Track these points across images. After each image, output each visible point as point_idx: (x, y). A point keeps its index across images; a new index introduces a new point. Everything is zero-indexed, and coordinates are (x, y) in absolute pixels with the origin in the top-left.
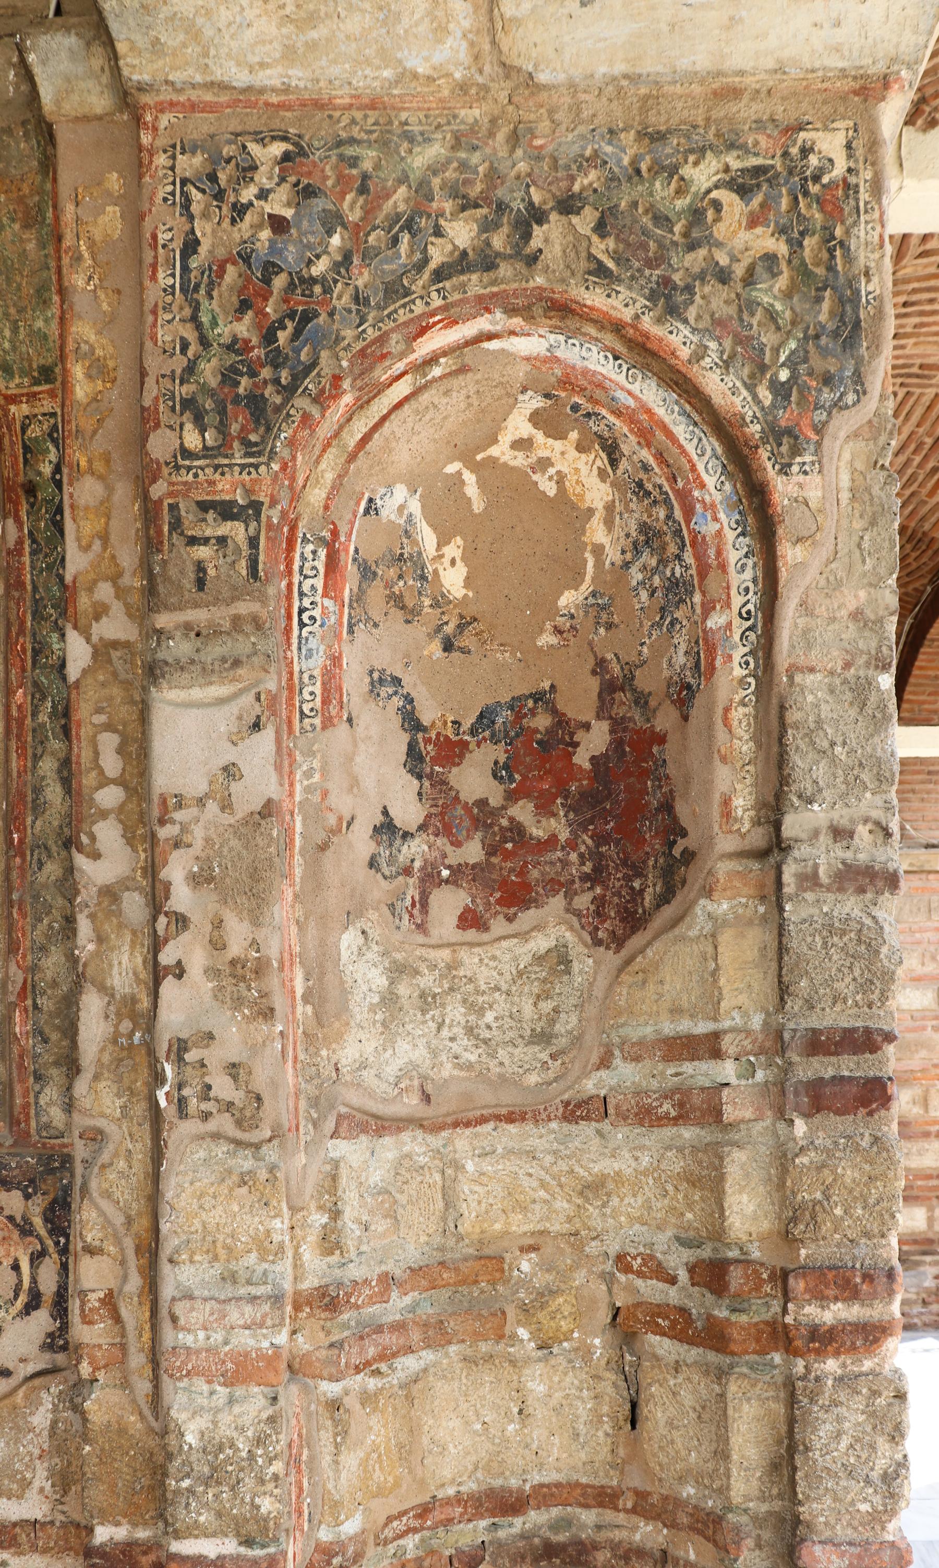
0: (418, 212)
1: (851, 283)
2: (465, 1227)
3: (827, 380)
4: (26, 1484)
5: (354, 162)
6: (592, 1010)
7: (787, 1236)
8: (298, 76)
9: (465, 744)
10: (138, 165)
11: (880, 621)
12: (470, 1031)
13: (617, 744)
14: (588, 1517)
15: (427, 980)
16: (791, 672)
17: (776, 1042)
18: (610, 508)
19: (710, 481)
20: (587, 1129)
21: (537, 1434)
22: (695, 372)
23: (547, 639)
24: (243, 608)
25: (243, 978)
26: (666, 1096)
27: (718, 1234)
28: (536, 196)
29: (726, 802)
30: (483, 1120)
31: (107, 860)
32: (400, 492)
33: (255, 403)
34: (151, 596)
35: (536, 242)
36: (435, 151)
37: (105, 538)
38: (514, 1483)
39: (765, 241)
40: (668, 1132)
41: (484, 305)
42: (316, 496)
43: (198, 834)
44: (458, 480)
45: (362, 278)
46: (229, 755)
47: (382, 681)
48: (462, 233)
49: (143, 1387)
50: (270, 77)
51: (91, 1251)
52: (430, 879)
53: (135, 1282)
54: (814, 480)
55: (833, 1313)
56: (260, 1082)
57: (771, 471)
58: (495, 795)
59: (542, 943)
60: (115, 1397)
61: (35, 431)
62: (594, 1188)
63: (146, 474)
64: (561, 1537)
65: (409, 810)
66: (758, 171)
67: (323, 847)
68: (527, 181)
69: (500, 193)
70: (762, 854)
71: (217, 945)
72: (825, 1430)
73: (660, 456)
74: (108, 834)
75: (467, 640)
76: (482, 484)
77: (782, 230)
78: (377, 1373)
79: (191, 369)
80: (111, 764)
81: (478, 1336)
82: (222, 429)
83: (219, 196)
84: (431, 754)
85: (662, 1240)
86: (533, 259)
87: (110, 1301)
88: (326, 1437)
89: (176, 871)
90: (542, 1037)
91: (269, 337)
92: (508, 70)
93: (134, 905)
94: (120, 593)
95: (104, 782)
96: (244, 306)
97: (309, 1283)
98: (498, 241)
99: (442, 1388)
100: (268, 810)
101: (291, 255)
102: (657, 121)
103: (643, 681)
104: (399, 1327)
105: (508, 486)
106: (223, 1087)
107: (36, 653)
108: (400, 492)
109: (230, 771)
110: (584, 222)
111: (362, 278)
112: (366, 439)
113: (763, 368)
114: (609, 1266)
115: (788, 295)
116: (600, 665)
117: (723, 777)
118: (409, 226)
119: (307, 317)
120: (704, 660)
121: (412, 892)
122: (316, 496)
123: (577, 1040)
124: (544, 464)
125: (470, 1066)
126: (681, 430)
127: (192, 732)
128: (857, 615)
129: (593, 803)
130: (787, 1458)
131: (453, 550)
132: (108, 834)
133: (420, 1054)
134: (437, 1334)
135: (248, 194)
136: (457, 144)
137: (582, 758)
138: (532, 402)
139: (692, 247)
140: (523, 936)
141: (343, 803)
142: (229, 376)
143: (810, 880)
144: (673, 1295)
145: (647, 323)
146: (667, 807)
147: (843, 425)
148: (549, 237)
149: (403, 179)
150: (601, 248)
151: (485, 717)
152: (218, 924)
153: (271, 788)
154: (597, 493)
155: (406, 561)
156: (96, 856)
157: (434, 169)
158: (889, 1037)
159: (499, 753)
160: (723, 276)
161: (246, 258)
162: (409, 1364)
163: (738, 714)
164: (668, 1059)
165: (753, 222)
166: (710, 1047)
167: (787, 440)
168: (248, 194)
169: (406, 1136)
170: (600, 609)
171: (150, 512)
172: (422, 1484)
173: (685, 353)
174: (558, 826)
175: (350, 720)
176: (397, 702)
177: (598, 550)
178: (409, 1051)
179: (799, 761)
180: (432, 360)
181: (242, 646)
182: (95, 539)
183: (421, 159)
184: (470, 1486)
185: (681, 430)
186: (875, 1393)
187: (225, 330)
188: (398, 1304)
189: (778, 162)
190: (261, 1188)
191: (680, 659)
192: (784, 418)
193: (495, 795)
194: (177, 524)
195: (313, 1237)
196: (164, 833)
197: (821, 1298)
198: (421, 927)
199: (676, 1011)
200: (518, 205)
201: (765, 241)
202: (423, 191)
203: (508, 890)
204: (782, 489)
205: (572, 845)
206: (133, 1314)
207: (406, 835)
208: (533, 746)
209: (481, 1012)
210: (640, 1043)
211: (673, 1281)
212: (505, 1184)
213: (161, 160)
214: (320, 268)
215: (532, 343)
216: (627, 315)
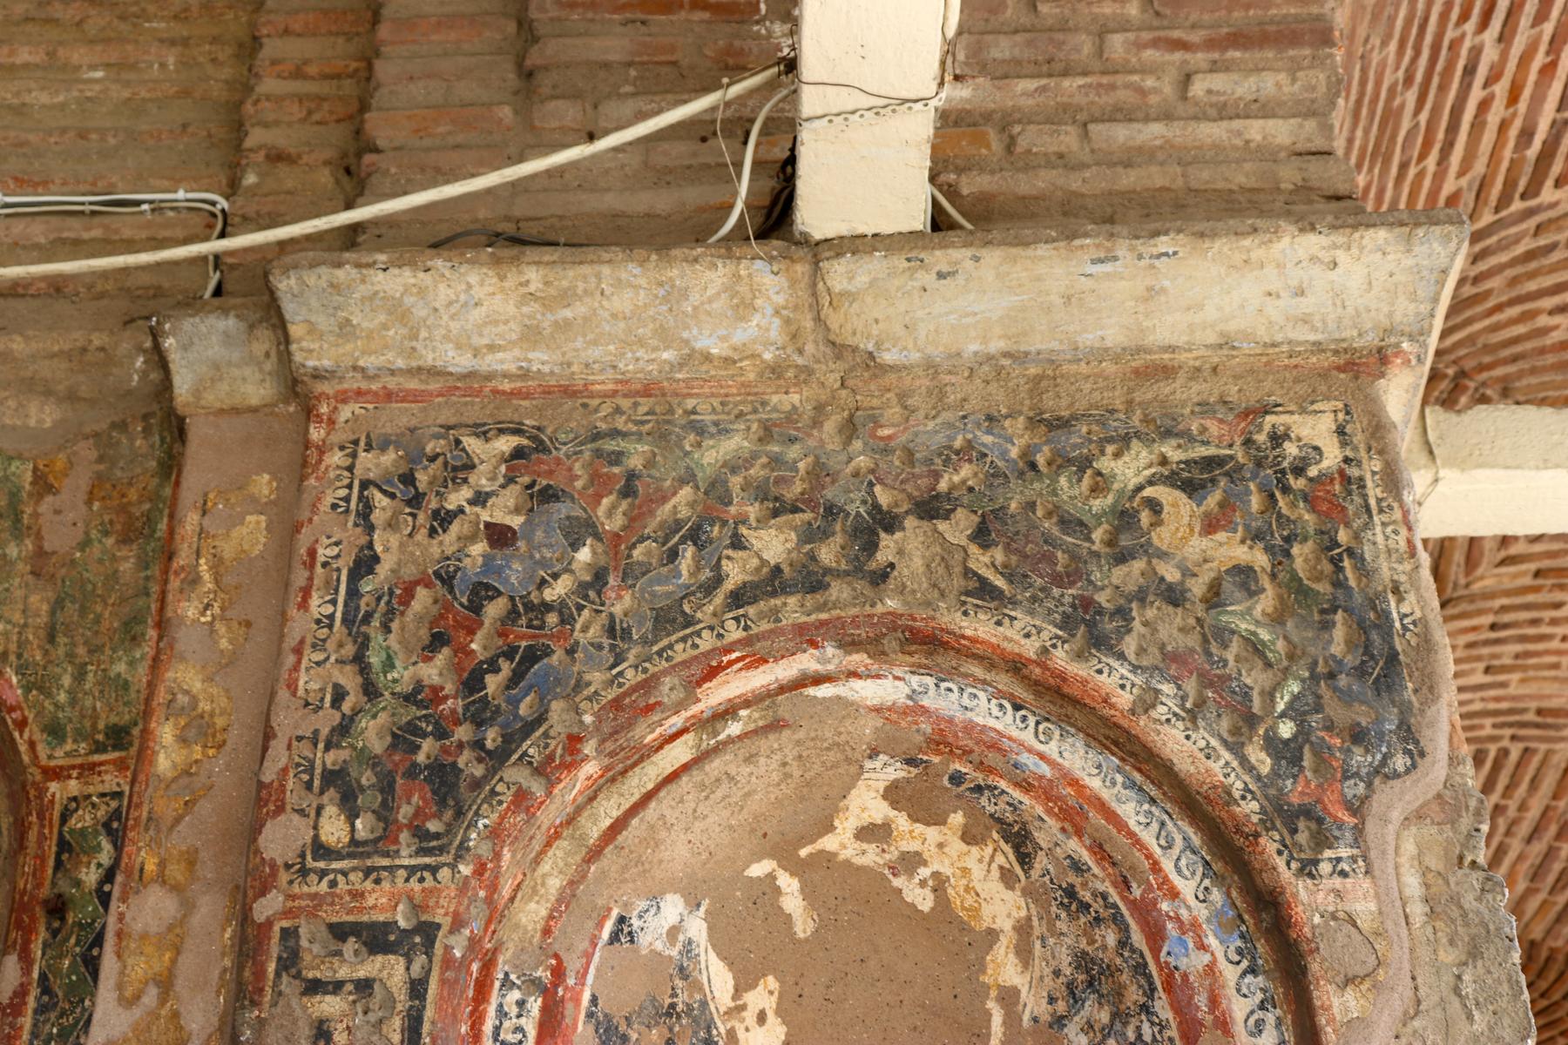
3: (1358, 736)
5: (616, 458)
8: (541, 360)
10: (304, 461)
18: (1023, 928)
19: (1187, 888)
28: (884, 497)
32: (673, 908)
33: (443, 779)
35: (884, 555)
36: (736, 443)
37: (166, 984)
41: (807, 637)
42: (531, 914)
45: (621, 603)
48: (774, 544)
50: (503, 361)
57: (1285, 873)
61: (83, 820)
66: (1210, 463)
68: (873, 477)
73: (1098, 849)
77: (1256, 536)
79: (344, 728)
82: (385, 814)
83: (416, 501)
86: (881, 577)
92: (839, 349)
96: (437, 641)
98: (827, 554)
101: (515, 574)
105: (851, 896)
108: (673, 908)
110: (958, 528)
111: (621, 603)
113: (1251, 720)
115: (1277, 619)
118: (694, 536)
119: (533, 656)
122: (531, 914)
126: (1130, 811)
131: (762, 997)
136: (768, 433)
138: (888, 771)
139: (1122, 558)
142: (403, 739)
145: (1061, 658)
147: (1394, 804)
148: (906, 548)
149: (688, 478)
150: (982, 561)
154: (1002, 907)
160: (1174, 596)
165: (1210, 526)
168: (457, 498)
171: (248, 940)
173: (1124, 699)
177: (1009, 997)
180: (728, 712)
183: (712, 455)
185: (1130, 811)
187: (404, 675)
192: (1295, 792)
194: (290, 961)
200: (856, 507)
204: (1309, 900)
214: (558, 590)
215: (884, 689)
216: (1030, 648)
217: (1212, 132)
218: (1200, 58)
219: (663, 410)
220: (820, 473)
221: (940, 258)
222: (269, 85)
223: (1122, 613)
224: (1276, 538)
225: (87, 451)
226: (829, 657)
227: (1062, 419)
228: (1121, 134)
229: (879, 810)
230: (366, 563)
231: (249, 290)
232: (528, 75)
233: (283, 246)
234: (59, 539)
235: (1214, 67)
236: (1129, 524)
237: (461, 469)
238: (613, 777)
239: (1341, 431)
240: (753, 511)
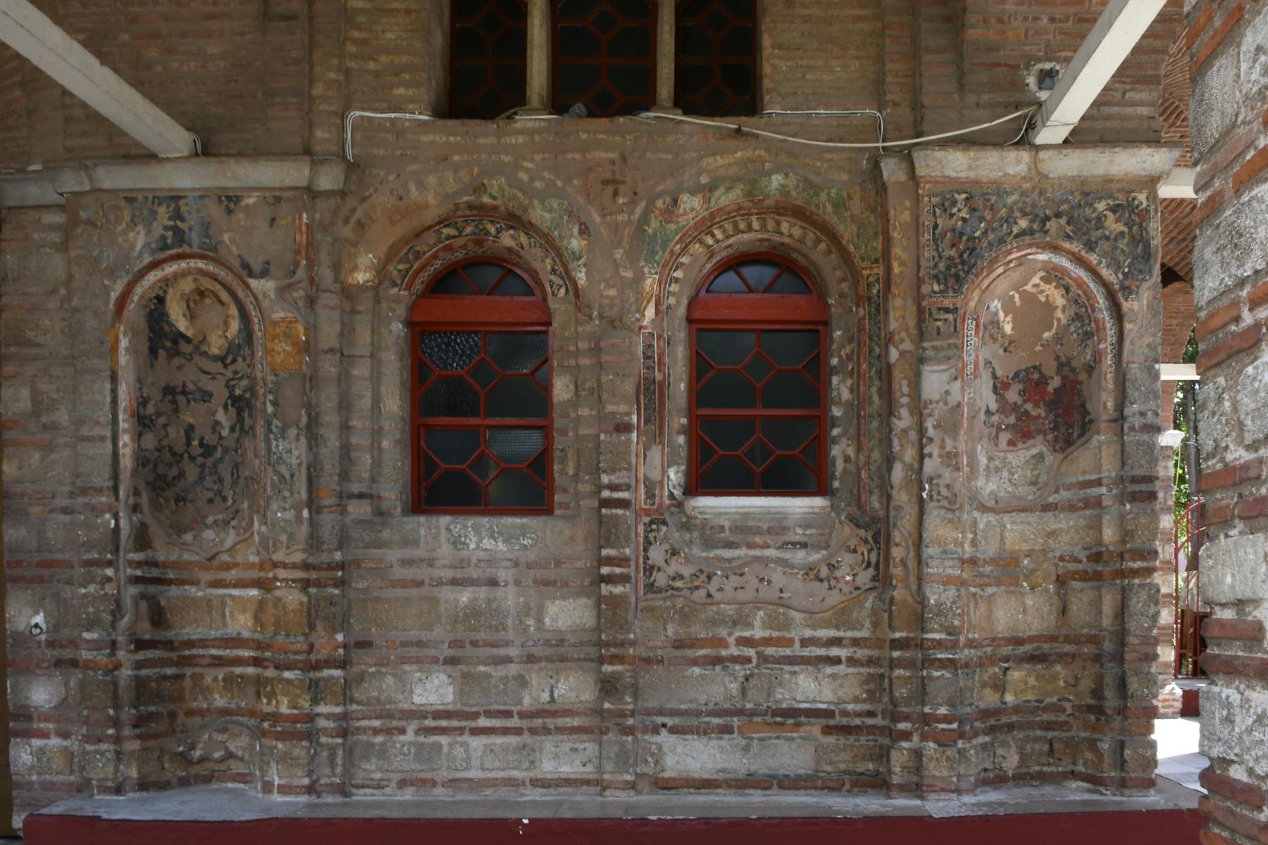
0: (1009, 217)
1: (1148, 241)
2: (1007, 547)
3: (1140, 272)
4: (863, 626)
5: (989, 200)
6: (1052, 474)
7: (1123, 542)
8: (972, 174)
10: (917, 200)
11: (1156, 347)
12: (1010, 480)
13: (1064, 385)
14: (1046, 646)
15: (997, 463)
16: (1128, 363)
17: (1121, 480)
18: (1064, 307)
19: (1101, 301)
20: (1050, 514)
21: (1029, 619)
22: (1098, 268)
23: (1038, 348)
24: (951, 341)
25: (950, 458)
26: (1081, 500)
27: (1100, 543)
28: (1047, 212)
29: (1105, 404)
31: (903, 420)
32: (996, 302)
33: (957, 277)
34: (921, 336)
35: (1047, 227)
37: (903, 317)
39: (1121, 227)
40: (1081, 513)
41: (1030, 246)
42: (972, 304)
43: (937, 412)
44: (1013, 297)
46: (947, 387)
47: (988, 363)
48: (1023, 223)
49: (914, 587)
50: (963, 175)
51: (896, 545)
52: (999, 429)
53: (912, 554)
54: (1136, 303)
55: (1138, 564)
56: (956, 489)
57: (1122, 300)
58: (1019, 401)
59: (1034, 451)
60: (904, 591)
61: (871, 279)
62: (1052, 534)
63: (919, 298)
64: (1038, 653)
65: (994, 406)
66: (1119, 205)
67: (974, 417)
68: (1045, 207)
69: (1036, 211)
70: (1115, 421)
71: (943, 447)
72: (1134, 601)
73: (1085, 293)
74: (904, 412)
75: (1011, 349)
77: (1126, 224)
79: (936, 266)
80: (905, 390)
81: (1011, 584)
82: (946, 284)
83: (945, 211)
84: (999, 387)
85: (1077, 549)
87: (903, 562)
88: (972, 605)
89: (929, 424)
90: (1034, 483)
91: (961, 255)
92: (1039, 173)
93: (913, 435)
94: (909, 335)
95: (903, 395)
96: (953, 245)
97: (967, 556)
98: (1035, 226)
99: (999, 600)
100: (959, 405)
101: (968, 229)
102: (1086, 189)
103: (1074, 363)
106: (944, 492)
107: (870, 352)
108: (996, 302)
109: (947, 393)
110: (1063, 221)
111: (991, 237)
114: (1056, 561)
115: (1127, 245)
116: (1058, 358)
117: (1104, 396)
119: (973, 249)
120: (1097, 357)
121: (994, 433)
122: (972, 304)
123: (1046, 484)
124: (1042, 292)
126: (1092, 285)
127: (934, 381)
128: (1149, 345)
129: (1057, 403)
130: (1122, 612)
131: (1008, 319)
132: (904, 412)
133: (994, 487)
134: (998, 583)
135: (955, 210)
136: (1022, 195)
137: (1050, 389)
138: (1042, 274)
139: (1097, 229)
140: (1028, 449)
141: (979, 402)
142: (948, 268)
143: (1132, 429)
144: (1081, 567)
145: (1083, 253)
146: (1083, 405)
147: (1145, 285)
148: (1052, 225)
149: (1005, 206)
150: (1068, 229)
151: (1017, 374)
152: (943, 441)
153: (960, 399)
154: (1060, 301)
155: (996, 324)
156: (900, 419)
157: (1015, 203)
158: (1157, 478)
159: (1021, 386)
160: (1107, 238)
161: (954, 230)
163: (1109, 376)
164: (1080, 488)
165: (1117, 221)
166: (1098, 483)
167: (1127, 291)
168: (955, 210)
170: (1058, 338)
171: (920, 310)
172: (992, 631)
174: (1041, 411)
177: (1059, 320)
178: (992, 486)
179: (1130, 391)
180: (1011, 261)
181: (951, 353)
182: (900, 315)
183: (1010, 200)
184: (1006, 635)
185: (1092, 285)
187: (946, 254)
188: (988, 569)
190: (955, 523)
191: (1088, 357)
192: (1126, 283)
193: (1019, 401)
194: (931, 315)
195: (968, 541)
196: (926, 412)
197: (1134, 561)
198: (996, 445)
199: (1084, 473)
201: (1121, 227)
202: (1011, 210)
203: (1023, 433)
204: (1126, 306)
205: (1046, 418)
206: (911, 564)
208: (1032, 382)
210: (1071, 484)
211: (1080, 562)
212: (1017, 532)
213: (926, 199)
214: (977, 234)
215: (1043, 257)
216: (1076, 250)
217: (1129, 110)
218: (1128, 87)
219: (998, 188)
220: (1034, 205)
221: (1065, 151)
222: (889, 79)
223: (1096, 243)
225: (858, 188)
227: (1088, 191)
230: (936, 226)
231: (907, 156)
232: (962, 85)
233: (917, 144)
234: (856, 211)
235: (1132, 90)
236: (1100, 219)
237: (954, 203)
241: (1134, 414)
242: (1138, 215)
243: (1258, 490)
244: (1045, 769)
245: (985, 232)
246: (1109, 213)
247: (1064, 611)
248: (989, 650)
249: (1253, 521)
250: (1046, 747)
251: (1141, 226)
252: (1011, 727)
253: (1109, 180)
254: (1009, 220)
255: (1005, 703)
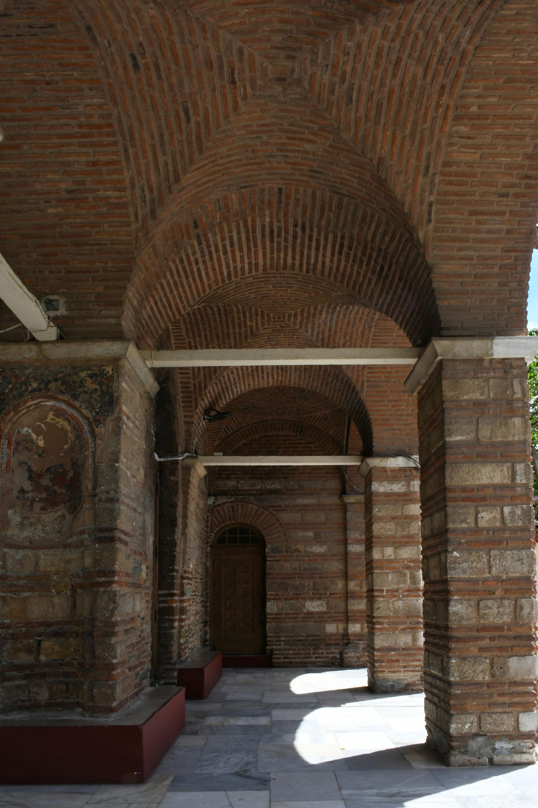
3: (106, 411)
9: (43, 475)
12: (43, 530)
14: (66, 627)
15: (32, 520)
19: (86, 428)
23: (62, 454)
28: (50, 378)
29: (87, 486)
30: (46, 548)
36: (31, 370)
38: (50, 620)
39: (96, 386)
41: (39, 397)
42: (6, 430)
44: (40, 426)
45: (15, 393)
48: (35, 385)
55: (103, 579)
57: (94, 427)
58: (50, 484)
59: (60, 513)
62: (68, 561)
66: (94, 374)
67: (4, 495)
76: (45, 426)
77: (99, 384)
78: (15, 594)
86: (49, 390)
90: (59, 532)
92: (45, 357)
98: (42, 386)
104: (22, 586)
105: (51, 426)
110: (59, 383)
111: (15, 393)
112: (17, 420)
113: (93, 409)
116: (72, 460)
118: (25, 384)
122: (6, 430)
124: (58, 422)
125: (42, 537)
126: (80, 419)
128: (112, 453)
131: (40, 438)
133: (30, 534)
134: (32, 589)
137: (68, 477)
139: (80, 387)
140: (56, 512)
143: (100, 500)
145: (71, 401)
149: (24, 375)
150: (62, 388)
151: (48, 470)
154: (69, 428)
157: (30, 374)
159: (52, 476)
160: (86, 393)
162: (26, 594)
163: (90, 470)
165: (93, 383)
167: (97, 422)
169: (26, 550)
173: (78, 406)
174: (63, 490)
175: (12, 471)
176: (26, 467)
177: (70, 438)
183: (27, 372)
185: (80, 419)
186: (110, 594)
189: (98, 373)
192: (97, 418)
193: (50, 484)
197: (100, 577)
198: (31, 510)
200: (46, 380)
201: (96, 386)
202: (28, 377)
204: (97, 430)
207: (27, 492)
209: (46, 527)
214: (7, 391)
216: (67, 399)
217: (103, 321)
218: (103, 308)
221: (58, 345)
223: (79, 395)
224: (101, 384)
226: (43, 400)
227: (75, 366)
228: (89, 321)
229: (53, 417)
235: (105, 309)
236: (82, 383)
238: (16, 414)
239: (113, 370)
240: (33, 380)
241: (102, 492)
242: (106, 379)
243: (523, 509)
244: (65, 700)
245: (11, 390)
246: (87, 378)
247: (74, 605)
248: (24, 630)
249: (349, 541)
250: (65, 687)
251: (108, 385)
252: (43, 675)
253: (89, 360)
254: (27, 383)
255: (40, 661)
